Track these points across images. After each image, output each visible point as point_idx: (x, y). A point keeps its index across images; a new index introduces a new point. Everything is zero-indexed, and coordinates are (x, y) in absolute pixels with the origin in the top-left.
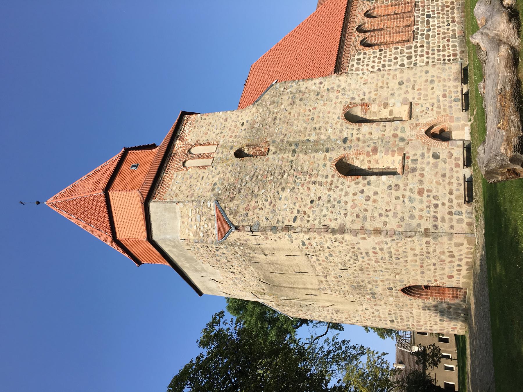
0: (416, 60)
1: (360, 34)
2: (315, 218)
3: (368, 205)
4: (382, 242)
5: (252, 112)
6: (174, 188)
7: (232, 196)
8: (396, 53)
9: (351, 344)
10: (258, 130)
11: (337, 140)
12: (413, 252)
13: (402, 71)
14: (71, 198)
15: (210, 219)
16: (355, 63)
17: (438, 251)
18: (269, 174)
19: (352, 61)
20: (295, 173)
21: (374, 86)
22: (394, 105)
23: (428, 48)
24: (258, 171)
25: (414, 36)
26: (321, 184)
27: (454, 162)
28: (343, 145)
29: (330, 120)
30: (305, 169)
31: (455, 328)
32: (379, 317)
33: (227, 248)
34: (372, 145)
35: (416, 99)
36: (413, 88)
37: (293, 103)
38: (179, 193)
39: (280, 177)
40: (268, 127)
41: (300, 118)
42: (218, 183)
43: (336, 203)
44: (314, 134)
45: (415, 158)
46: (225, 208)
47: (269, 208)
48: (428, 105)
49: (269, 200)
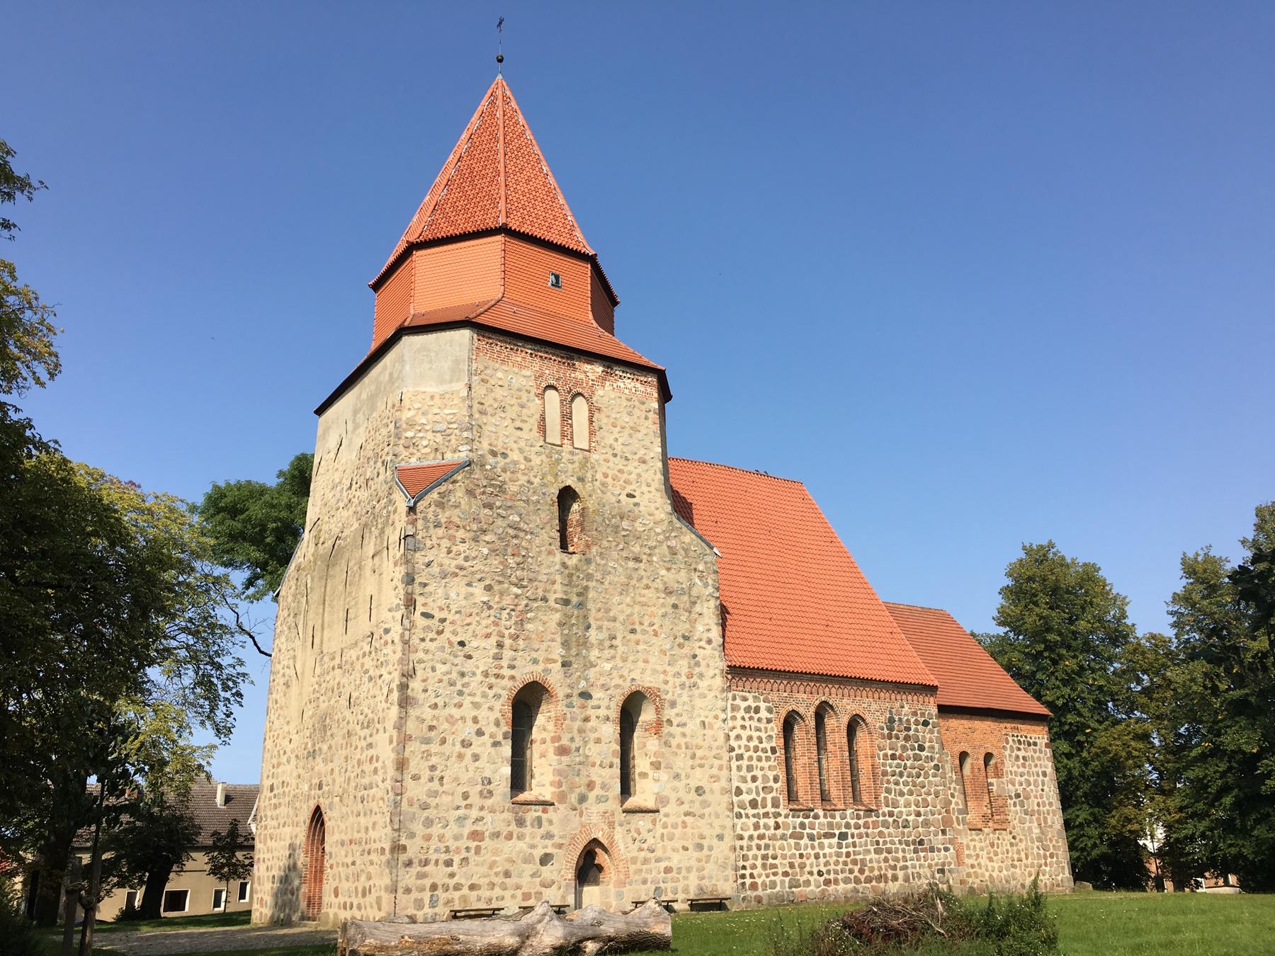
0: (747, 816)
1: (812, 709)
2: (430, 652)
3: (454, 745)
4: (385, 773)
5: (656, 512)
6: (499, 375)
7: (478, 491)
8: (765, 778)
9: (234, 708)
10: (616, 529)
11: (587, 680)
12: (370, 826)
13: (726, 791)
14: (501, 146)
15: (436, 450)
16: (751, 702)
17: (371, 869)
18: (519, 559)
19: (755, 697)
20: (520, 608)
21: (699, 741)
22: (657, 780)
23: (773, 838)
24: (529, 537)
25: (801, 810)
26: (498, 657)
27: (533, 891)
28: (576, 692)
29: (629, 665)
30: (529, 626)
31: (261, 901)
32: (279, 764)
33: (386, 483)
34: (573, 746)
35: (664, 819)
36: (686, 814)
37: (668, 592)
38: (488, 385)
39: (513, 579)
40: (621, 547)
41: (637, 608)
42: (507, 460)
43: (459, 687)
44: (601, 636)
45: (545, 823)
46: (454, 482)
47: (451, 564)
48: (651, 841)
49: (466, 564)
